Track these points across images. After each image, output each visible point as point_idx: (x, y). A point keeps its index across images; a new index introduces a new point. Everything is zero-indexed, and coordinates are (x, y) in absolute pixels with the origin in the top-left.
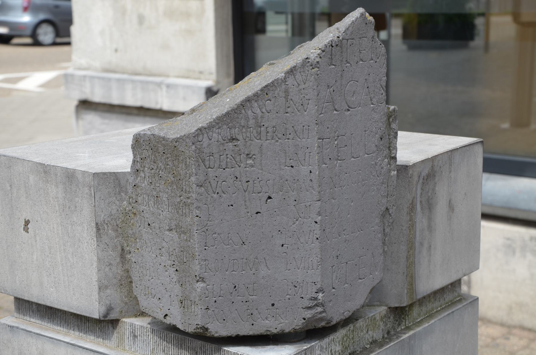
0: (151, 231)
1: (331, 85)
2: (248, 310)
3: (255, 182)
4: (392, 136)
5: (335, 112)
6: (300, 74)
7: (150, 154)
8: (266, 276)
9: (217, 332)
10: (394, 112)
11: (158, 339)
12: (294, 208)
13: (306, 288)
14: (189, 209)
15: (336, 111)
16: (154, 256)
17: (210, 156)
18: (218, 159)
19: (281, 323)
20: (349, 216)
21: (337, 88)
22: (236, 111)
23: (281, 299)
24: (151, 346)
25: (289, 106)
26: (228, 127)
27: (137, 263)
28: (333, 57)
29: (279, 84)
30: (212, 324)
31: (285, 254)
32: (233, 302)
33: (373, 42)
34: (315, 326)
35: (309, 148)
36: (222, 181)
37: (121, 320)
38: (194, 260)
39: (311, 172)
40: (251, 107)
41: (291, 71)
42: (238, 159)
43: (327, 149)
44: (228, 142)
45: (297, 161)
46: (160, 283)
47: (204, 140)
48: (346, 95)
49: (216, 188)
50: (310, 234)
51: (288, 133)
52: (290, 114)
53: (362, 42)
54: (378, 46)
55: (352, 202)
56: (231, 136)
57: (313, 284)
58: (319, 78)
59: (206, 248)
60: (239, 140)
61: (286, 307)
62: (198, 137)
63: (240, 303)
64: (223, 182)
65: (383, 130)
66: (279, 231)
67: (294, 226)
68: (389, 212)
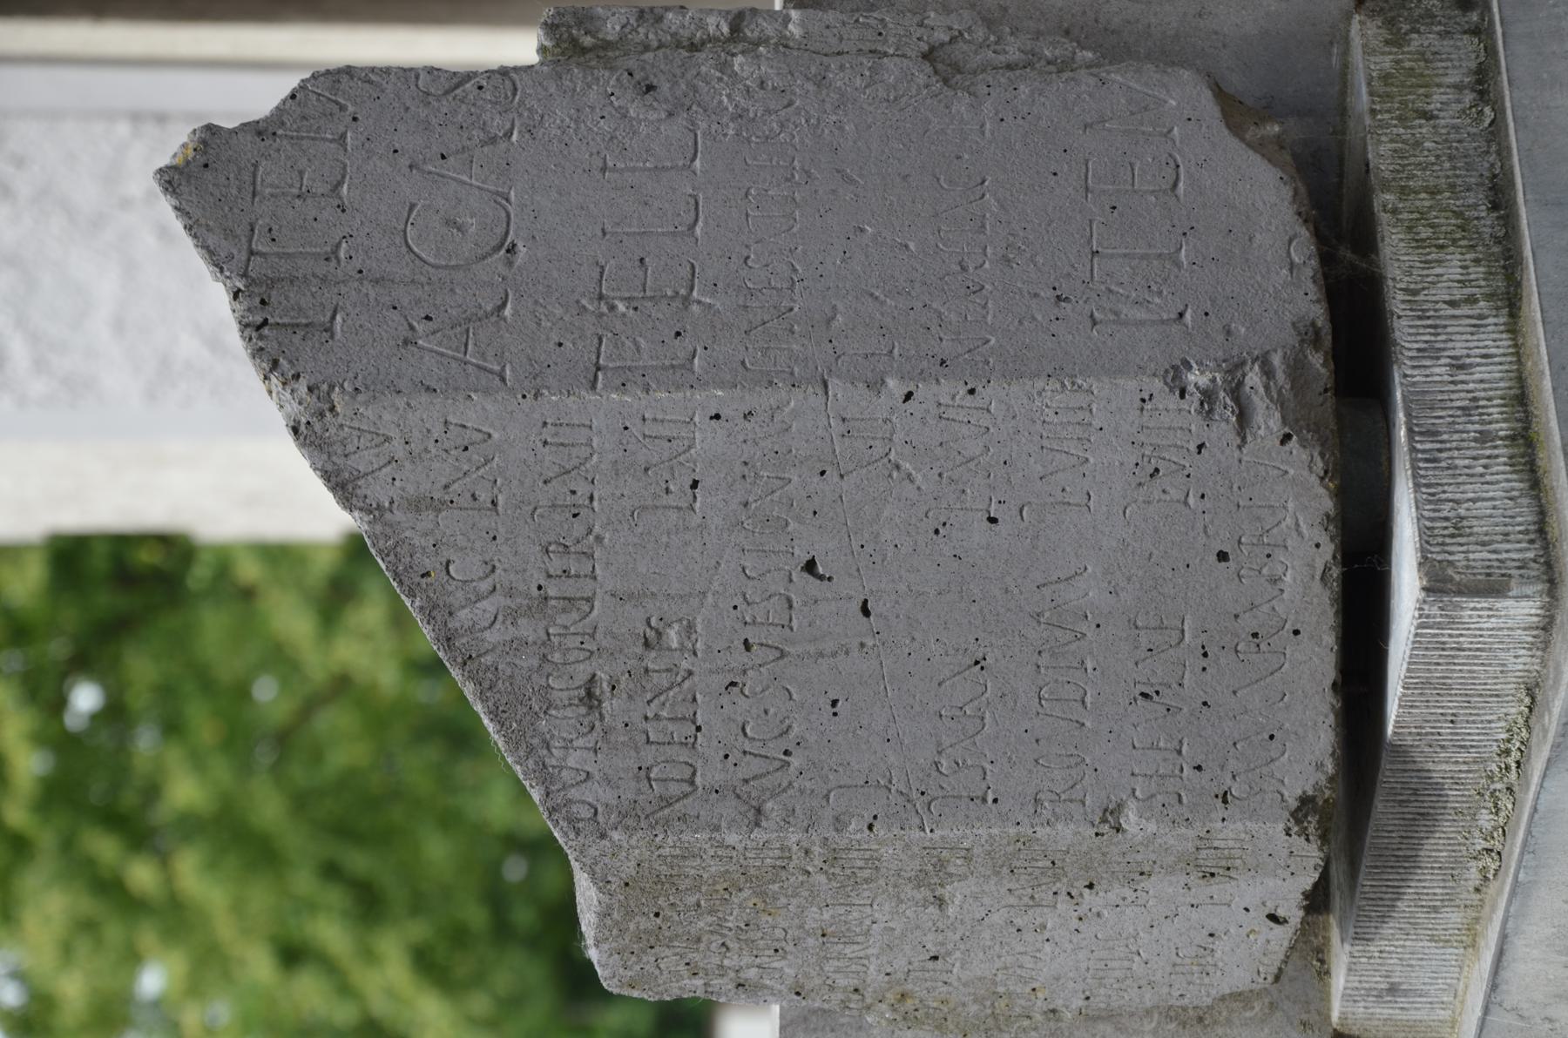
0: (958, 954)
1: (404, 331)
2: (1239, 648)
3: (748, 619)
4: (651, 36)
5: (508, 312)
6: (353, 457)
7: (668, 952)
8: (1110, 582)
9: (1319, 766)
10: (557, 26)
11: (1391, 925)
12: (852, 479)
13: (1164, 432)
14: (849, 849)
15: (504, 305)
16: (1048, 947)
17: (649, 779)
18: (661, 749)
19: (1297, 525)
20: (912, 246)
21: (418, 301)
22: (486, 684)
23: (1199, 525)
24: (1421, 944)
25: (469, 495)
26: (545, 712)
27: (1088, 993)
28: (304, 321)
29: (388, 531)
30: (1286, 780)
31: (1024, 513)
32: (1205, 704)
33: (280, 132)
34: (1326, 391)
35: (628, 425)
36: (741, 738)
37: (1335, 1026)
38: (1038, 840)
39: (717, 417)
40: (471, 630)
41: (343, 488)
42: (663, 680)
43: (638, 350)
44: (601, 714)
45: (672, 468)
46: (1151, 933)
47: (590, 800)
48: (453, 263)
49: (766, 757)
50: (953, 420)
51: (569, 499)
52: (500, 492)
53: (271, 186)
54: (299, 110)
55: (862, 230)
56: (576, 702)
57: (1148, 406)
58: (367, 388)
59: (990, 799)
60: (594, 676)
61: (1234, 509)
62: (579, 820)
63: (1207, 676)
64: (745, 734)
65: (618, 80)
66: (937, 532)
67: (919, 478)
68: (942, 45)
